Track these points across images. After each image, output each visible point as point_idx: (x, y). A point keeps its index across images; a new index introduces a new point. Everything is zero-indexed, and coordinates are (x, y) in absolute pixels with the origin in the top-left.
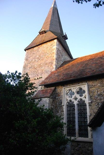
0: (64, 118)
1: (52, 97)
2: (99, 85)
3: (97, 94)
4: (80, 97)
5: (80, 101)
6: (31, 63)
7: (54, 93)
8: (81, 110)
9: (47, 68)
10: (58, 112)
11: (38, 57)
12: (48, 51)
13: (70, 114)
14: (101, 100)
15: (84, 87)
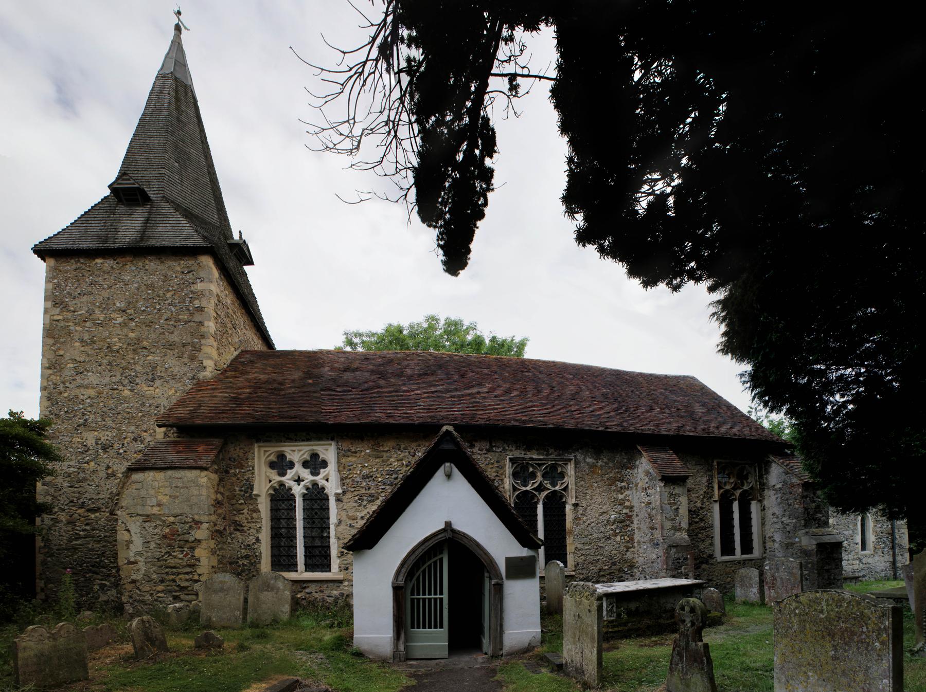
1: (216, 467)
2: (368, 451)
4: (310, 475)
5: (310, 487)
6: (88, 324)
8: (313, 509)
10: (239, 512)
14: (369, 489)
15: (324, 452)
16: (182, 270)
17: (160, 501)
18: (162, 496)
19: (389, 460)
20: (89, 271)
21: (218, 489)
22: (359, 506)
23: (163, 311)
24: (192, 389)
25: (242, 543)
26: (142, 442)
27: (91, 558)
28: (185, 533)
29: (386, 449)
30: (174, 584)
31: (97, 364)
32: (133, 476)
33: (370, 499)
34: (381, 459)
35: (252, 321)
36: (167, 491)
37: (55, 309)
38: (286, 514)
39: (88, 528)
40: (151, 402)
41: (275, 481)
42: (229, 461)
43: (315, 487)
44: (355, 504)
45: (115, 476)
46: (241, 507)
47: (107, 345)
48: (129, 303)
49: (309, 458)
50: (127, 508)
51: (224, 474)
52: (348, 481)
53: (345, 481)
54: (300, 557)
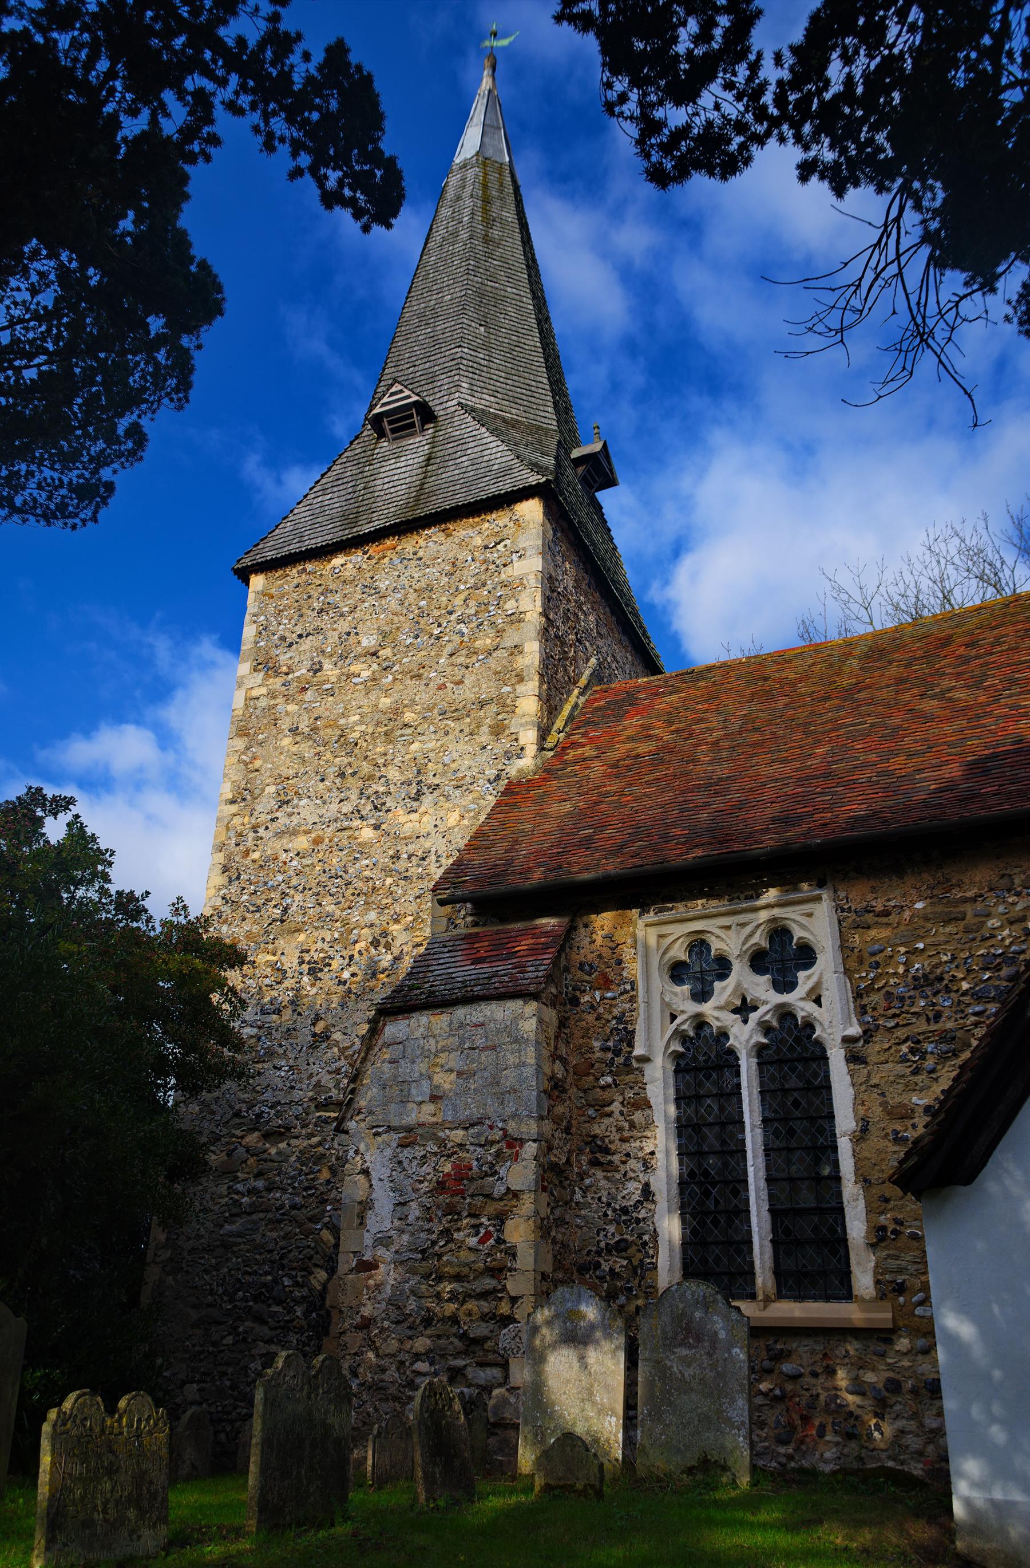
0: (653, 1153)
1: (554, 990)
2: (919, 905)
3: (907, 971)
4: (772, 992)
5: (775, 1023)
6: (309, 696)
7: (563, 962)
8: (785, 1091)
9: (461, 746)
10: (602, 1107)
11: (368, 641)
12: (462, 597)
13: (697, 1128)
14: (938, 1016)
15: (803, 920)
16: (486, 542)
17: (438, 1087)
18: (441, 1075)
19: (984, 923)
20: (320, 585)
21: (556, 1048)
22: (916, 1072)
23: (447, 638)
24: (498, 804)
25: (609, 1205)
26: (388, 947)
27: (255, 1273)
28: (486, 1175)
29: (969, 894)
30: (454, 1330)
31: (319, 777)
32: (387, 1029)
33: (944, 1047)
34: (962, 923)
35: (613, 613)
36: (454, 1060)
37: (256, 674)
38: (716, 1108)
39: (260, 1184)
40: (411, 848)
41: (684, 1017)
42: (579, 974)
43: (787, 1024)
44: (901, 1069)
45: (328, 1038)
46: (606, 1095)
47: (340, 732)
48: (384, 635)
49: (765, 944)
50: (370, 1113)
51: (568, 1006)
52: (875, 998)
53: (865, 1001)
54: (761, 1246)
